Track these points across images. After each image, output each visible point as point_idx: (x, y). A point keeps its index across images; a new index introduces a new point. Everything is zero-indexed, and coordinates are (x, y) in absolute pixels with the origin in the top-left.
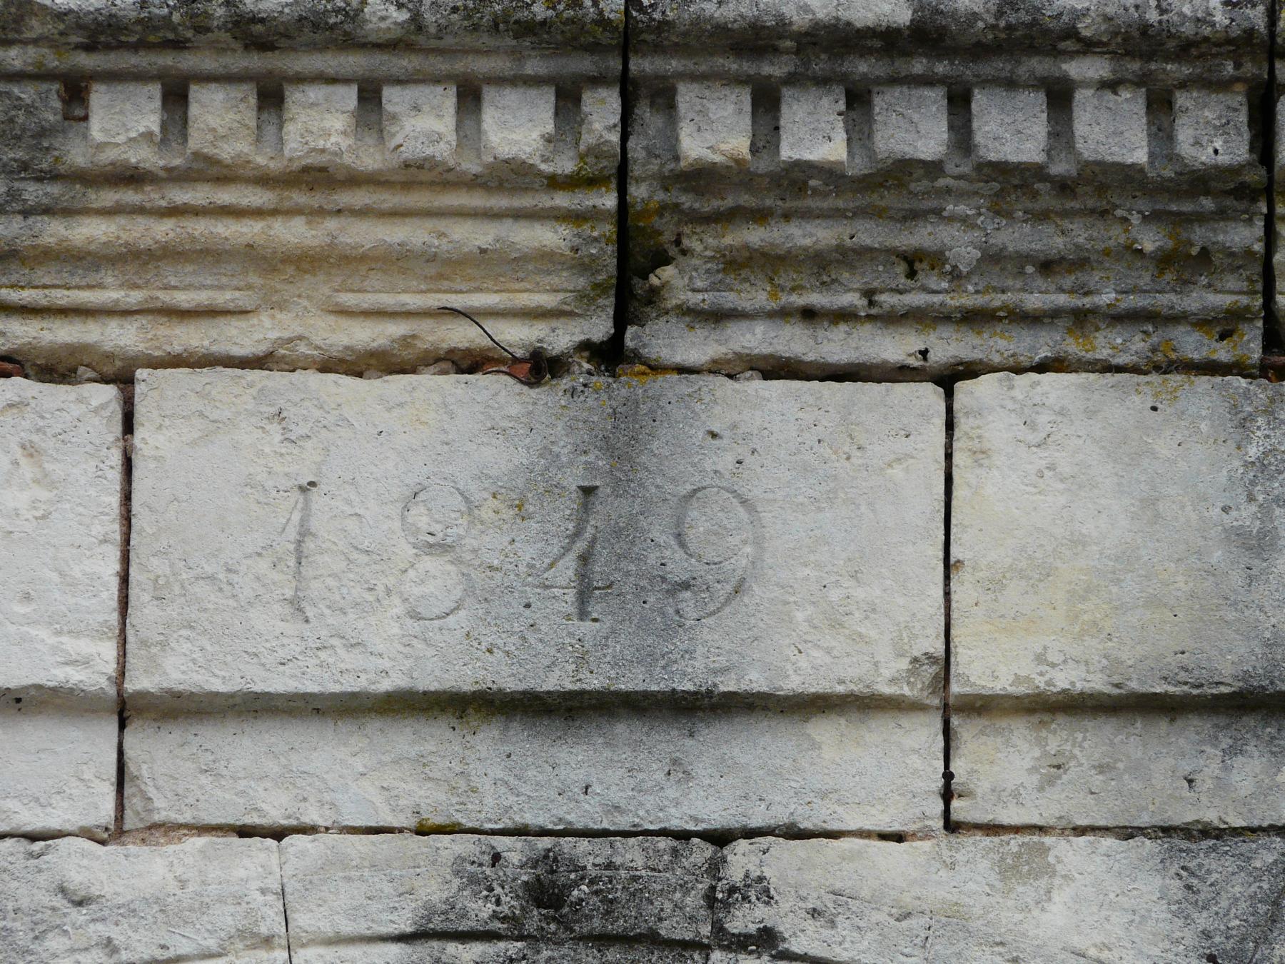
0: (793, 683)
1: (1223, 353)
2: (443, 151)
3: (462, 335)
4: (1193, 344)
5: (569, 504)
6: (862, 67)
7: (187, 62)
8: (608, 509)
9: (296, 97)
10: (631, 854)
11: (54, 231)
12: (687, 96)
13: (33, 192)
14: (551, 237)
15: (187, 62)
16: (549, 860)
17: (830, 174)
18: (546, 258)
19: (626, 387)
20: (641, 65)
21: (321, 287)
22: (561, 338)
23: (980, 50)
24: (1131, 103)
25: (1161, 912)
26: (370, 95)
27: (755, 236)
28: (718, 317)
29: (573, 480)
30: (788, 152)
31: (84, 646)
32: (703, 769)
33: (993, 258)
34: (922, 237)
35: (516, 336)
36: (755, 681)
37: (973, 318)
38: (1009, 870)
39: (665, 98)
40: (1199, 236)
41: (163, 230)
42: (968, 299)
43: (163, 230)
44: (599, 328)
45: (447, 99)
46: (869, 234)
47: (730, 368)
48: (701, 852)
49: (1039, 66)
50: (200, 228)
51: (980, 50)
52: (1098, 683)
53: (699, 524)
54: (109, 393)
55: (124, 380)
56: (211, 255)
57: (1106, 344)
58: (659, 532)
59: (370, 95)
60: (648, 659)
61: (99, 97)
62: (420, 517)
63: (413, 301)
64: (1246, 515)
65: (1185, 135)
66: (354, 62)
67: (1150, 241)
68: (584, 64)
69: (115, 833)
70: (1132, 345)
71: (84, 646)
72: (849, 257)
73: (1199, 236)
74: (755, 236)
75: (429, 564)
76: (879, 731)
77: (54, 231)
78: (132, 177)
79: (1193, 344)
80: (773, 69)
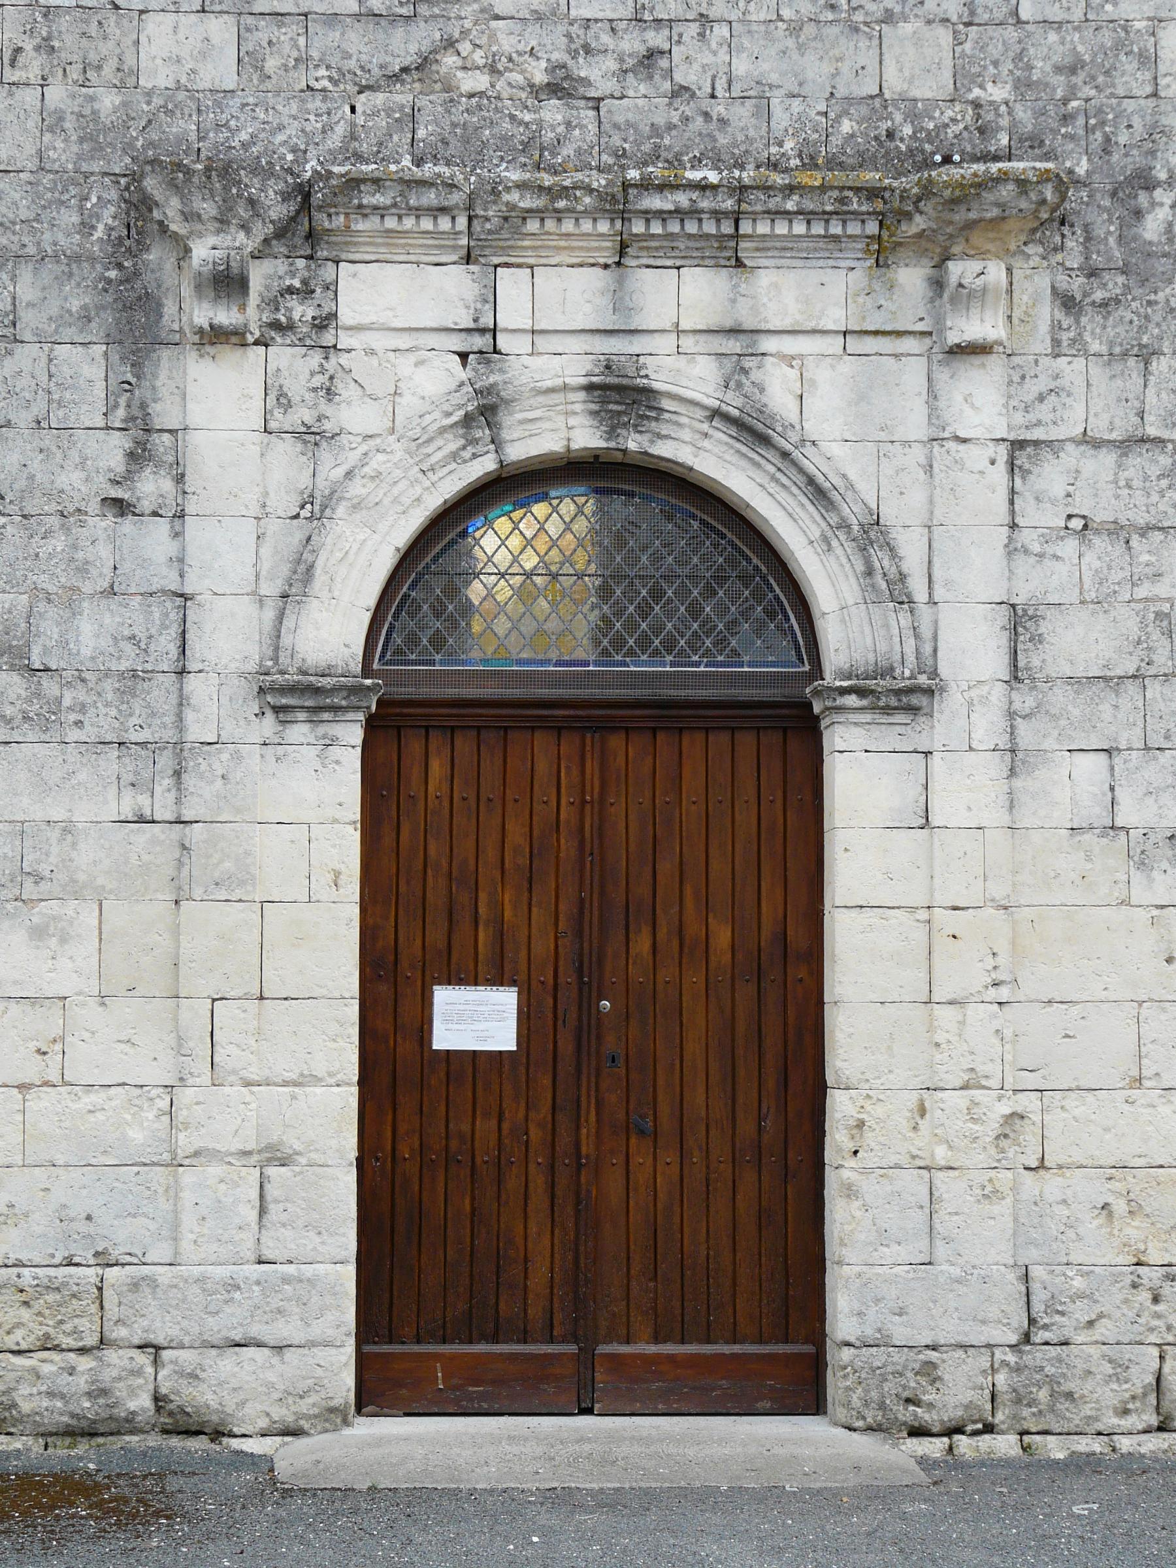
0: (651, 328)
1: (728, 264)
2: (590, 231)
3: (592, 261)
4: (723, 262)
5: (611, 293)
6: (665, 216)
7: (544, 215)
8: (618, 294)
9: (564, 221)
10: (623, 358)
11: (520, 243)
12: (633, 220)
13: (516, 236)
14: (609, 244)
15: (544, 215)
16: (608, 360)
17: (659, 235)
18: (608, 248)
19: (621, 270)
20: (626, 215)
21: (567, 252)
22: (610, 261)
23: (686, 213)
24: (713, 221)
25: (715, 370)
26: (577, 220)
27: (645, 244)
28: (638, 257)
29: (612, 288)
30: (652, 232)
31: (526, 321)
32: (635, 343)
33: (687, 248)
34: (674, 244)
35: (602, 261)
36: (645, 328)
37: (683, 257)
38: (688, 362)
39: (630, 220)
40: (724, 244)
41: (539, 243)
42: (683, 254)
43: (539, 243)
44: (617, 259)
45: (591, 221)
46: (665, 244)
47: (639, 267)
48: (635, 358)
49: (697, 215)
50: (546, 243)
51: (686, 213)
52: (705, 328)
53: (634, 297)
54: (529, 270)
55: (532, 267)
56: (549, 247)
57: (707, 262)
58: (627, 299)
59: (577, 220)
60: (626, 323)
61: (528, 221)
62: (585, 296)
63: (631, 839)
64: (731, 295)
65: (722, 228)
66: (574, 215)
67: (716, 245)
68: (615, 216)
69: (532, 354)
70: (712, 262)
71: (526, 321)
72: (662, 247)
73: (724, 244)
74: (645, 244)
75: (588, 305)
76: (666, 335)
77: (520, 243)
78: (534, 234)
79: (723, 262)
80: (649, 216)
